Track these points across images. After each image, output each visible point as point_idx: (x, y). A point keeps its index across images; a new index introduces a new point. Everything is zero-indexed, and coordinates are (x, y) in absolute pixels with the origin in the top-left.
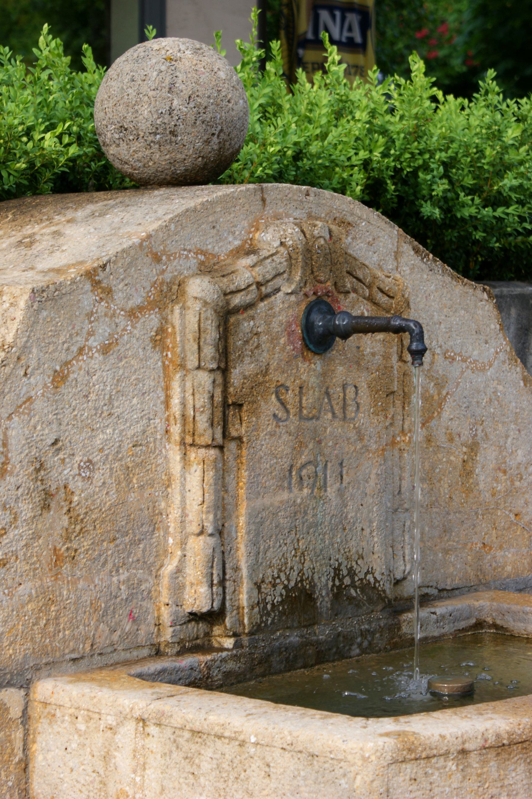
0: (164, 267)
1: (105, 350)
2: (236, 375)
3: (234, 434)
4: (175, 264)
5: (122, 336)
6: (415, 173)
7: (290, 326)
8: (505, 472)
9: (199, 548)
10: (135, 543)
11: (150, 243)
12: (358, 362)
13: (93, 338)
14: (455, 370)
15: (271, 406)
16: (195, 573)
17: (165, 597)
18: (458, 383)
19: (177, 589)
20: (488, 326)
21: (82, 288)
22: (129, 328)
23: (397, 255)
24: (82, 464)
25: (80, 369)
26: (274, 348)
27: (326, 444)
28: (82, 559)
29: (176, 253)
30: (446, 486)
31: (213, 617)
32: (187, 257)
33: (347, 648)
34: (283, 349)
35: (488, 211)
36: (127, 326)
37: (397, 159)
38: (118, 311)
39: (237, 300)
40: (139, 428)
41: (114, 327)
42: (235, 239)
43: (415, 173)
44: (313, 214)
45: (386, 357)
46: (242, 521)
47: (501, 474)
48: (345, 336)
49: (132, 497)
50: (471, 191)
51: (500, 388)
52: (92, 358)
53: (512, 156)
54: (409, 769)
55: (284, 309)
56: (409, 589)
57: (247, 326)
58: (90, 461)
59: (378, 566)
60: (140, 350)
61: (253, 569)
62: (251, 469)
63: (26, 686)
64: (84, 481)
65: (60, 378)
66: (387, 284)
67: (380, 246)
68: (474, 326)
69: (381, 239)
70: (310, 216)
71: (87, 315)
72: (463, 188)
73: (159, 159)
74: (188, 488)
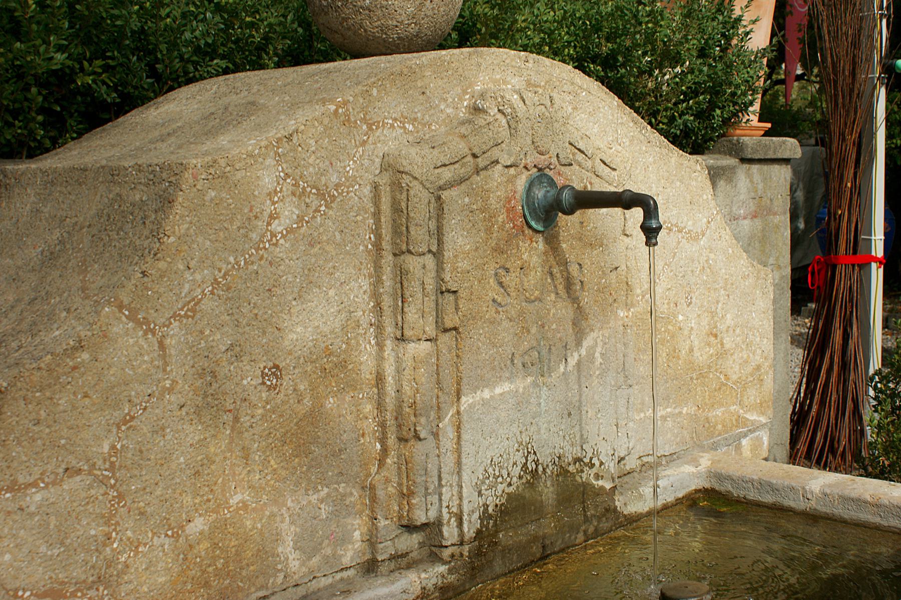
0: (365, 138)
3: (449, 324)
4: (378, 134)
5: (314, 217)
7: (509, 202)
8: (716, 336)
11: (348, 110)
13: (277, 221)
18: (675, 254)
20: (701, 196)
21: (262, 163)
22: (323, 208)
24: (267, 370)
25: (261, 258)
26: (493, 225)
27: (549, 327)
29: (379, 122)
30: (664, 355)
32: (392, 126)
33: (573, 537)
34: (502, 228)
36: (321, 206)
38: (309, 189)
41: (304, 208)
42: (448, 106)
44: (532, 81)
47: (713, 339)
51: (712, 256)
52: (276, 245)
56: (631, 463)
58: (276, 367)
60: (337, 233)
64: (269, 390)
68: (689, 197)
69: (602, 110)
70: (529, 83)
71: (269, 194)
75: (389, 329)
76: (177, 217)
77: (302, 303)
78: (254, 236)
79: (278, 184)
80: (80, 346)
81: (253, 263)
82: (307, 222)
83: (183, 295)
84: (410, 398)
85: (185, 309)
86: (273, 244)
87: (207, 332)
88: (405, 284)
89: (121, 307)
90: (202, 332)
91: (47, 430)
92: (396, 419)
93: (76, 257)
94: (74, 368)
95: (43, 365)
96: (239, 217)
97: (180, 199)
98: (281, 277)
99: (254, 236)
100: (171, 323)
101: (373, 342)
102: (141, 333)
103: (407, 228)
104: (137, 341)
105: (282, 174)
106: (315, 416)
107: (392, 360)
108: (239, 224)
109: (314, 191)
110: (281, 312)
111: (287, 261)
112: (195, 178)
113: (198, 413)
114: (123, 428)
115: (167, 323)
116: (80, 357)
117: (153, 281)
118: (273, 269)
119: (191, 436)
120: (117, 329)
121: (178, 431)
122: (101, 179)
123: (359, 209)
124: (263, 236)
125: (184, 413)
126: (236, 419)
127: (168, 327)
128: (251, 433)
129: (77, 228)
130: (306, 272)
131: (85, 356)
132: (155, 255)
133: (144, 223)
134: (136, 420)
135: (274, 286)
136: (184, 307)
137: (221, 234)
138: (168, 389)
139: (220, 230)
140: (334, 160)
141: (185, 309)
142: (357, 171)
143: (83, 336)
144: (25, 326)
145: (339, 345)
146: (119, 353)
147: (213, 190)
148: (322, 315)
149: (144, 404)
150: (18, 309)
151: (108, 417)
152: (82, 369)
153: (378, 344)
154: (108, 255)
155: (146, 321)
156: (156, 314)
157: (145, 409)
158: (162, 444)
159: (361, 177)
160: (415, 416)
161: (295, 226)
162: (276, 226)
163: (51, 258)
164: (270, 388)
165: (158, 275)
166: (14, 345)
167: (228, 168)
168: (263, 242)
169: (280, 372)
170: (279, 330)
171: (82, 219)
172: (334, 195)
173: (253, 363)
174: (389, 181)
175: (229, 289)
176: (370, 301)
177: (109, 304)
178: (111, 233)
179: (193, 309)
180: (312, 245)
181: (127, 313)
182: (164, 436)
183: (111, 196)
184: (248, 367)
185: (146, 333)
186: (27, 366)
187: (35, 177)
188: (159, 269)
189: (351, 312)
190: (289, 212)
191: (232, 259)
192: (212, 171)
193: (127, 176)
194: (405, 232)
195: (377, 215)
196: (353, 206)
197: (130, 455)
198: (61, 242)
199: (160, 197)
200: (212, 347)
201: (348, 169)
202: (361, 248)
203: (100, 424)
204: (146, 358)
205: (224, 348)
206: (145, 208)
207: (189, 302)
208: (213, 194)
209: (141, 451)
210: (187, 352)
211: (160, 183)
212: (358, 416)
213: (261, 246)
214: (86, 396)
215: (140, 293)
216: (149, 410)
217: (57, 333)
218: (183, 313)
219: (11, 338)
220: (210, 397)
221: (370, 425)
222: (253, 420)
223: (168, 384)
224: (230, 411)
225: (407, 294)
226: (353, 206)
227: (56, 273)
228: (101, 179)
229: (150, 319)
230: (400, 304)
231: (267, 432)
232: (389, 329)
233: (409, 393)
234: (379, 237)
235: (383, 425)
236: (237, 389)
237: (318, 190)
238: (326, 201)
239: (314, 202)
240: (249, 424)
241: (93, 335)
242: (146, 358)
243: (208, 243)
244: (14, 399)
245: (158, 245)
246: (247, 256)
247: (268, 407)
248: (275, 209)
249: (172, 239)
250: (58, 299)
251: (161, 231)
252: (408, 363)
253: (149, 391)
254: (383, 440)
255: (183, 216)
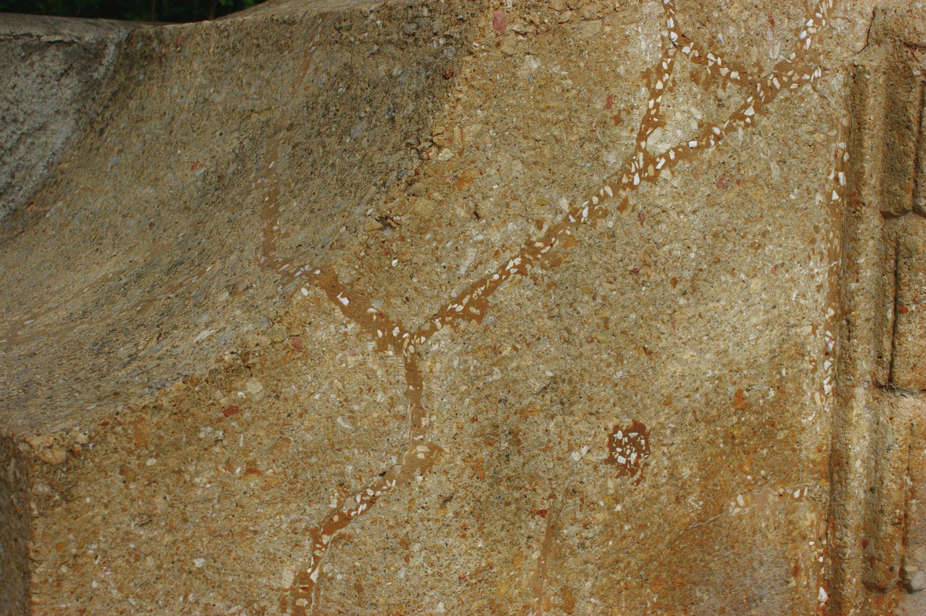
5: (731, 129)
13: (658, 132)
21: (636, 10)
22: (750, 112)
24: (619, 435)
25: (623, 207)
36: (746, 106)
38: (724, 71)
52: (653, 180)
58: (639, 427)
60: (773, 165)
71: (646, 75)
75: (864, 366)
76: (460, 108)
77: (698, 303)
78: (612, 158)
79: (666, 55)
80: (244, 365)
81: (606, 214)
82: (718, 138)
83: (463, 271)
84: (897, 506)
85: (465, 301)
86: (649, 179)
87: (507, 351)
88: (906, 277)
89: (333, 288)
90: (496, 350)
91: (168, 538)
92: (865, 544)
93: (262, 186)
94: (231, 411)
95: (165, 402)
96: (584, 117)
97: (467, 72)
98: (659, 246)
99: (612, 158)
100: (434, 328)
101: (828, 388)
102: (371, 345)
103: (917, 162)
104: (363, 364)
105: (674, 36)
106: (704, 532)
107: (864, 426)
108: (583, 132)
109: (734, 75)
110: (655, 317)
111: (673, 214)
112: (500, 28)
113: (478, 515)
114: (326, 539)
115: (427, 327)
116: (243, 388)
117: (402, 239)
118: (645, 230)
119: (461, 560)
120: (322, 334)
121: (436, 550)
122: (317, 39)
123: (820, 119)
124: (629, 160)
125: (450, 514)
126: (553, 530)
127: (428, 335)
128: (579, 559)
129: (270, 131)
130: (709, 239)
131: (255, 387)
132: (410, 184)
133: (392, 119)
134: (352, 524)
135: (646, 264)
136: (463, 295)
137: (546, 151)
138: (421, 462)
139: (545, 141)
140: (776, 15)
141: (465, 301)
142: (821, 41)
143: (252, 344)
144: (151, 315)
145: (762, 391)
146: (326, 386)
147: (536, 56)
148: (734, 328)
149: (370, 492)
150: (148, 280)
151: (294, 516)
152: (247, 415)
153: (836, 393)
154: (318, 181)
155: (384, 321)
156: (405, 308)
157: (372, 502)
158: (401, 575)
159: (828, 54)
160: (905, 542)
161: (693, 144)
162: (658, 143)
163: (218, 185)
164: (624, 470)
165: (413, 227)
166: (123, 352)
167: (569, 13)
168: (628, 173)
169: (646, 438)
170: (649, 353)
171: (277, 114)
172: (772, 87)
173: (593, 419)
174: (884, 64)
175: (555, 264)
176: (828, 305)
177: (310, 281)
178: (327, 140)
179: (479, 301)
180: (722, 185)
181: (345, 301)
182: (407, 559)
183: (334, 69)
184: (583, 426)
185: (381, 347)
186: (133, 402)
187: (207, 41)
188: (415, 213)
189: (789, 326)
190: (683, 116)
191: (564, 204)
192: (535, 16)
193: (363, 30)
194: (911, 170)
195: (855, 133)
196: (808, 112)
197: (335, 595)
198: (240, 158)
199: (427, 67)
200: (515, 381)
201: (803, 34)
202: (819, 198)
203: (278, 530)
204: (380, 397)
205: (538, 386)
206: (397, 90)
207: (474, 287)
208: (534, 64)
209: (359, 588)
210: (463, 388)
211: (428, 40)
212: (789, 534)
213: (625, 180)
214: (252, 469)
215: (376, 263)
216: (380, 503)
217: (205, 334)
218: (459, 308)
219: (122, 338)
220: (505, 483)
221: (811, 551)
222: (585, 534)
223: (421, 452)
224: (542, 513)
225: (907, 296)
226: (808, 112)
227: (223, 216)
228: (317, 39)
229: (393, 318)
230: (890, 315)
231: (610, 559)
232: (864, 366)
233: (895, 496)
234: (856, 178)
235: (835, 554)
236: (559, 470)
237: (743, 73)
238: (757, 97)
239: (734, 97)
240: (577, 540)
241: (273, 343)
242: (380, 397)
243: (520, 167)
244: (101, 469)
245: (416, 163)
246: (595, 200)
247: (619, 508)
248: (656, 106)
249: (446, 154)
250: (219, 265)
251: (425, 135)
252: (896, 437)
253: (383, 466)
254: (834, 584)
255: (471, 106)
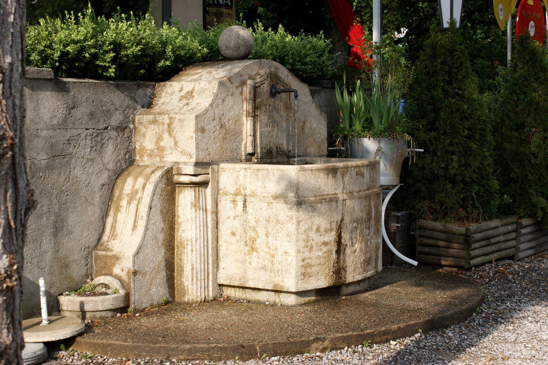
1: (232, 95)
2: (257, 101)
6: (284, 57)
9: (250, 139)
10: (237, 137)
12: (281, 100)
14: (300, 104)
15: (264, 109)
16: (249, 144)
17: (243, 149)
19: (246, 148)
23: (288, 76)
28: (228, 139)
31: (252, 154)
35: (303, 67)
37: (279, 53)
39: (257, 85)
40: (237, 112)
43: (284, 57)
45: (286, 99)
46: (258, 134)
48: (279, 93)
49: (237, 127)
50: (298, 62)
53: (308, 53)
54: (302, 172)
55: (266, 88)
57: (259, 90)
59: (285, 147)
61: (261, 144)
62: (260, 122)
63: (218, 165)
65: (224, 101)
66: (286, 82)
67: (284, 73)
72: (296, 61)
73: (235, 54)
74: (247, 125)
